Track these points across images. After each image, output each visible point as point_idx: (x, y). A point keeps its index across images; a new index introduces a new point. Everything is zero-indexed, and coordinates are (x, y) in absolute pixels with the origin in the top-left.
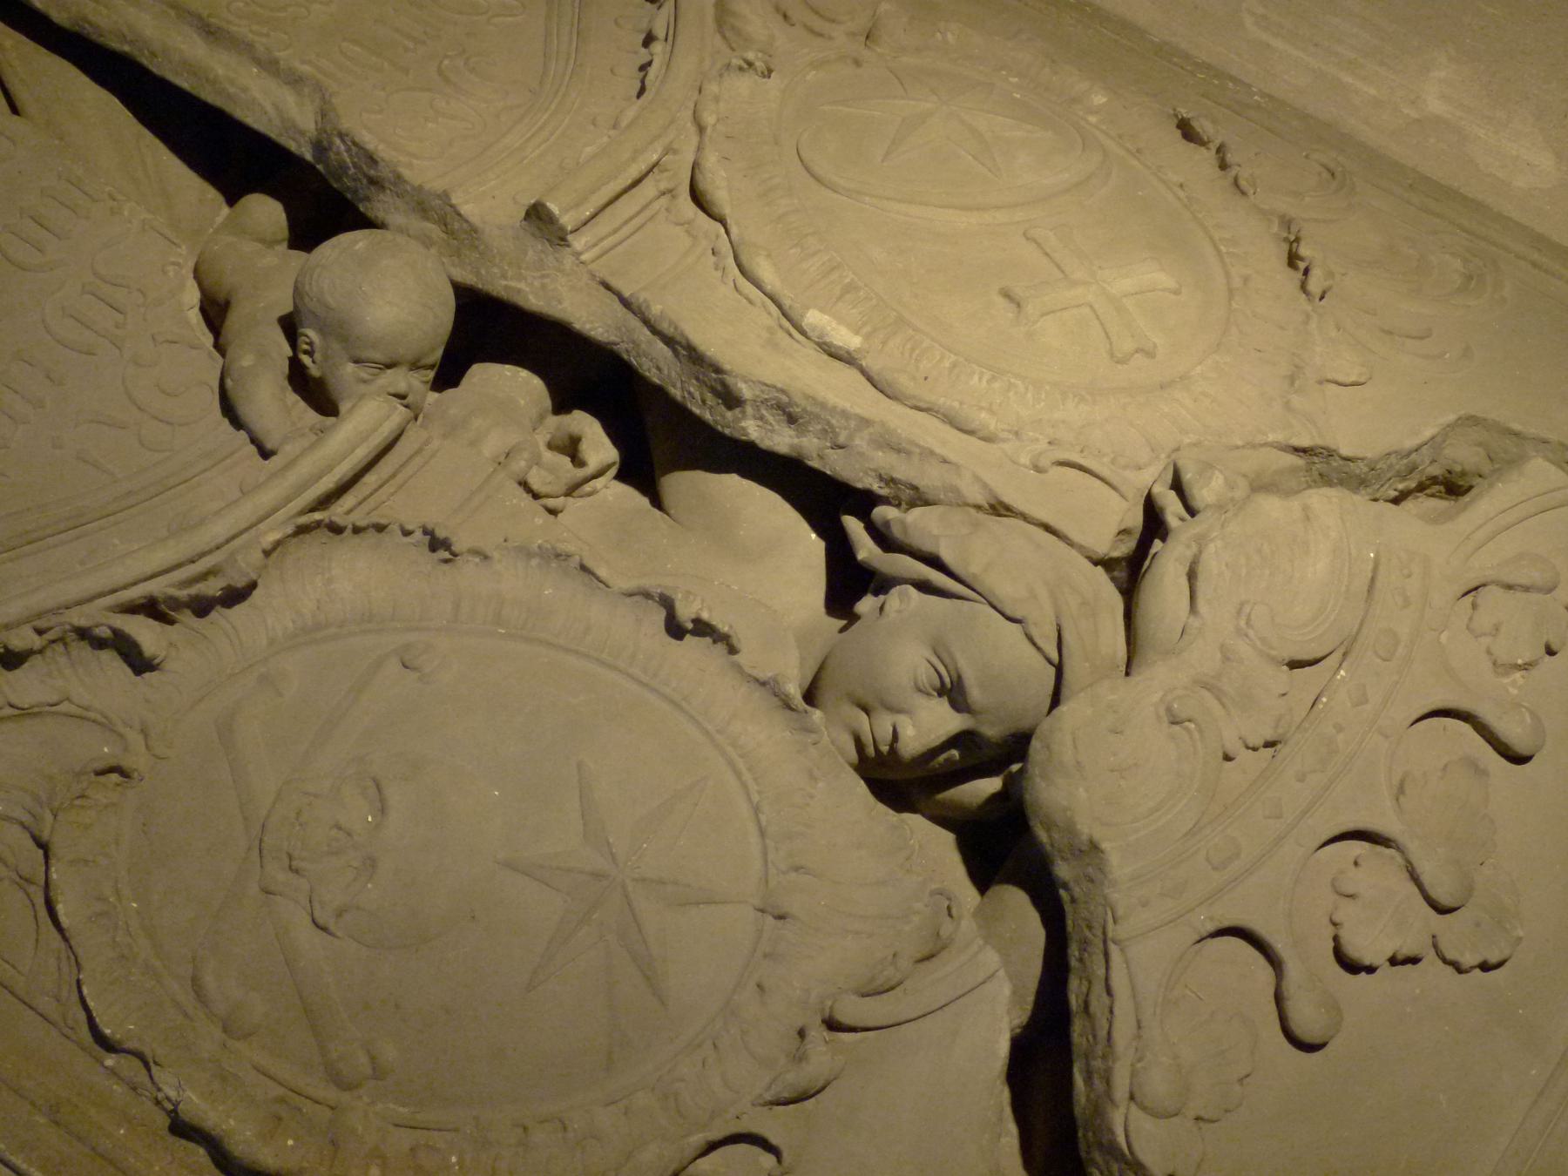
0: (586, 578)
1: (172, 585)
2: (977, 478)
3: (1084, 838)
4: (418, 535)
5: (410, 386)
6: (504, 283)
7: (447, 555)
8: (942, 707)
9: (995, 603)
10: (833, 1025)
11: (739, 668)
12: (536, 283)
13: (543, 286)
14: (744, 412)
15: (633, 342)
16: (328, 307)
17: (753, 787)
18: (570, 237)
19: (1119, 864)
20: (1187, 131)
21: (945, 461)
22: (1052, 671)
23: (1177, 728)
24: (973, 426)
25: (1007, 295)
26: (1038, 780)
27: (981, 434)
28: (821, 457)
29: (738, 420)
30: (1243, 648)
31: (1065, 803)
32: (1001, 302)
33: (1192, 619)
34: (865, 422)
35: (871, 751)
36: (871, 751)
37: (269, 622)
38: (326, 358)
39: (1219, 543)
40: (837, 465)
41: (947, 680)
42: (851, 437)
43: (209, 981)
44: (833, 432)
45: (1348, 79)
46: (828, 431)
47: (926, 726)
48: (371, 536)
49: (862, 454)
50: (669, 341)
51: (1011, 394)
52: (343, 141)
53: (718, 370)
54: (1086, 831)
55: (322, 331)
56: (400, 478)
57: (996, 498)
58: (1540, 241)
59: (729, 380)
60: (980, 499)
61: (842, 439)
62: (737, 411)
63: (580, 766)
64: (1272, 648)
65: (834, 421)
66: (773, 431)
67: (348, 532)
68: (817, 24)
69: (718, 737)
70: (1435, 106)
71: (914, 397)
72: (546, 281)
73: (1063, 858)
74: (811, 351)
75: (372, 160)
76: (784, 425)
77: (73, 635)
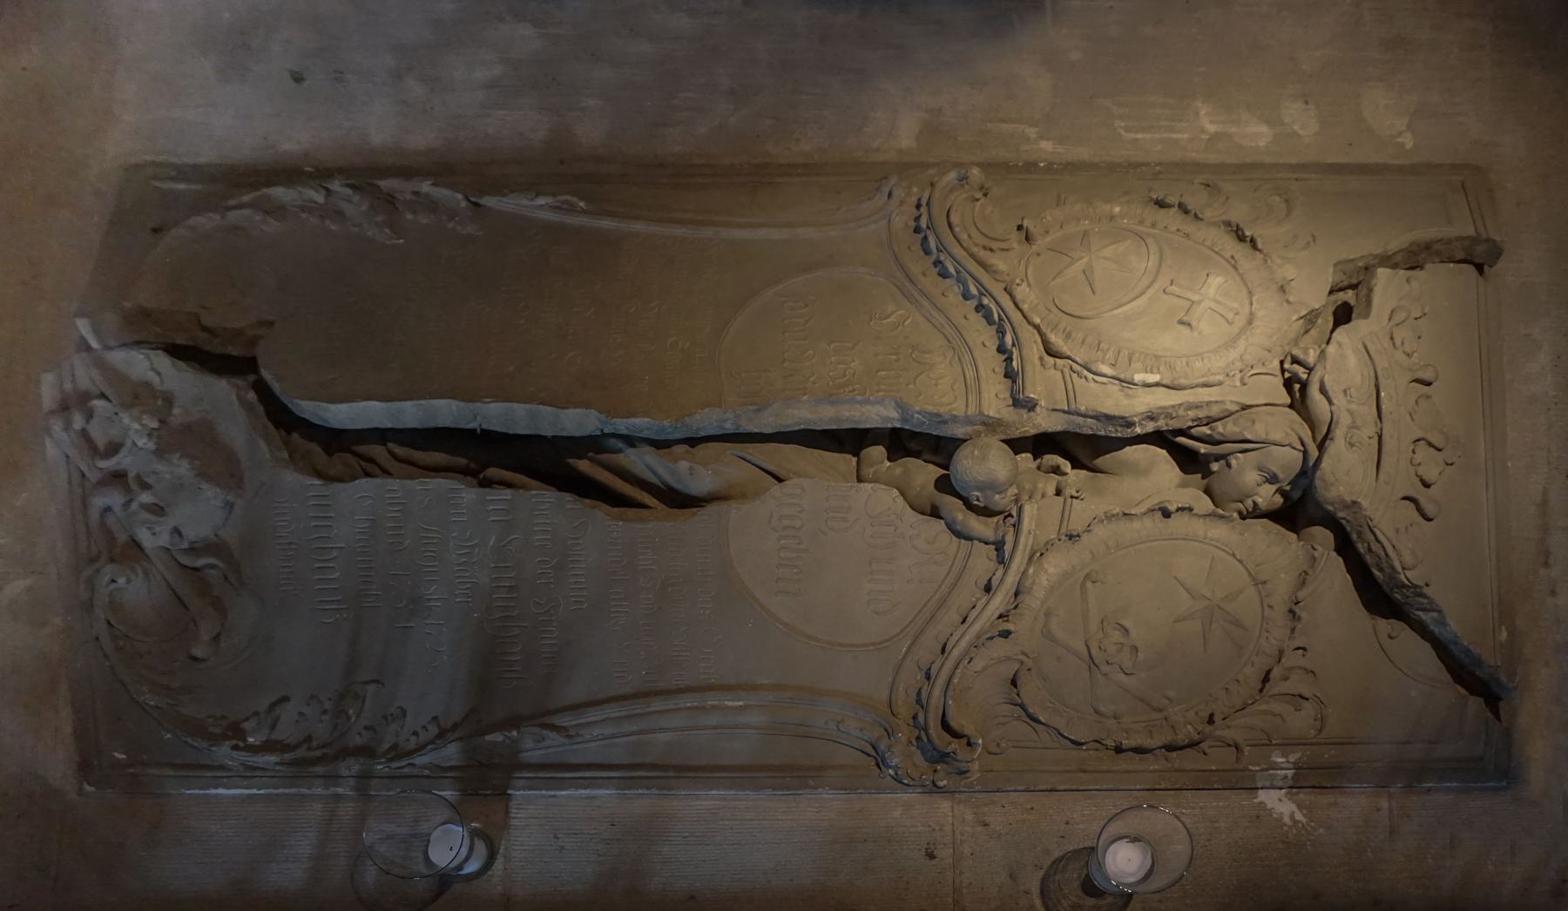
8: (1267, 486)
20: (1161, 204)
25: (1181, 322)
30: (1353, 406)
32: (1181, 327)
43: (1102, 709)
45: (1174, 136)
47: (1267, 496)
58: (1292, 168)
68: (1002, 245)
70: (1212, 128)
74: (1141, 390)
75: (938, 415)
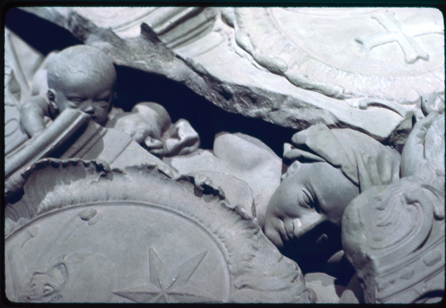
0: (161, 175)
2: (331, 113)
3: (140, 166)
5: (94, 108)
9: (328, 160)
11: (223, 205)
12: (149, 60)
13: (152, 61)
14: (233, 100)
17: (227, 254)
18: (160, 37)
19: (380, 268)
21: (317, 108)
23: (411, 206)
24: (333, 92)
27: (337, 96)
29: (232, 104)
31: (356, 242)
32: (355, 44)
34: (285, 97)
35: (286, 237)
36: (286, 237)
37: (30, 208)
39: (436, 126)
40: (277, 118)
42: (279, 105)
44: (271, 103)
46: (269, 104)
48: (71, 168)
49: (284, 111)
50: (201, 74)
51: (355, 80)
53: (220, 82)
56: (89, 146)
57: (338, 120)
59: (224, 86)
60: (332, 122)
61: (275, 106)
62: (231, 100)
65: (271, 99)
66: (247, 107)
67: (61, 167)
72: (153, 58)
76: (252, 104)
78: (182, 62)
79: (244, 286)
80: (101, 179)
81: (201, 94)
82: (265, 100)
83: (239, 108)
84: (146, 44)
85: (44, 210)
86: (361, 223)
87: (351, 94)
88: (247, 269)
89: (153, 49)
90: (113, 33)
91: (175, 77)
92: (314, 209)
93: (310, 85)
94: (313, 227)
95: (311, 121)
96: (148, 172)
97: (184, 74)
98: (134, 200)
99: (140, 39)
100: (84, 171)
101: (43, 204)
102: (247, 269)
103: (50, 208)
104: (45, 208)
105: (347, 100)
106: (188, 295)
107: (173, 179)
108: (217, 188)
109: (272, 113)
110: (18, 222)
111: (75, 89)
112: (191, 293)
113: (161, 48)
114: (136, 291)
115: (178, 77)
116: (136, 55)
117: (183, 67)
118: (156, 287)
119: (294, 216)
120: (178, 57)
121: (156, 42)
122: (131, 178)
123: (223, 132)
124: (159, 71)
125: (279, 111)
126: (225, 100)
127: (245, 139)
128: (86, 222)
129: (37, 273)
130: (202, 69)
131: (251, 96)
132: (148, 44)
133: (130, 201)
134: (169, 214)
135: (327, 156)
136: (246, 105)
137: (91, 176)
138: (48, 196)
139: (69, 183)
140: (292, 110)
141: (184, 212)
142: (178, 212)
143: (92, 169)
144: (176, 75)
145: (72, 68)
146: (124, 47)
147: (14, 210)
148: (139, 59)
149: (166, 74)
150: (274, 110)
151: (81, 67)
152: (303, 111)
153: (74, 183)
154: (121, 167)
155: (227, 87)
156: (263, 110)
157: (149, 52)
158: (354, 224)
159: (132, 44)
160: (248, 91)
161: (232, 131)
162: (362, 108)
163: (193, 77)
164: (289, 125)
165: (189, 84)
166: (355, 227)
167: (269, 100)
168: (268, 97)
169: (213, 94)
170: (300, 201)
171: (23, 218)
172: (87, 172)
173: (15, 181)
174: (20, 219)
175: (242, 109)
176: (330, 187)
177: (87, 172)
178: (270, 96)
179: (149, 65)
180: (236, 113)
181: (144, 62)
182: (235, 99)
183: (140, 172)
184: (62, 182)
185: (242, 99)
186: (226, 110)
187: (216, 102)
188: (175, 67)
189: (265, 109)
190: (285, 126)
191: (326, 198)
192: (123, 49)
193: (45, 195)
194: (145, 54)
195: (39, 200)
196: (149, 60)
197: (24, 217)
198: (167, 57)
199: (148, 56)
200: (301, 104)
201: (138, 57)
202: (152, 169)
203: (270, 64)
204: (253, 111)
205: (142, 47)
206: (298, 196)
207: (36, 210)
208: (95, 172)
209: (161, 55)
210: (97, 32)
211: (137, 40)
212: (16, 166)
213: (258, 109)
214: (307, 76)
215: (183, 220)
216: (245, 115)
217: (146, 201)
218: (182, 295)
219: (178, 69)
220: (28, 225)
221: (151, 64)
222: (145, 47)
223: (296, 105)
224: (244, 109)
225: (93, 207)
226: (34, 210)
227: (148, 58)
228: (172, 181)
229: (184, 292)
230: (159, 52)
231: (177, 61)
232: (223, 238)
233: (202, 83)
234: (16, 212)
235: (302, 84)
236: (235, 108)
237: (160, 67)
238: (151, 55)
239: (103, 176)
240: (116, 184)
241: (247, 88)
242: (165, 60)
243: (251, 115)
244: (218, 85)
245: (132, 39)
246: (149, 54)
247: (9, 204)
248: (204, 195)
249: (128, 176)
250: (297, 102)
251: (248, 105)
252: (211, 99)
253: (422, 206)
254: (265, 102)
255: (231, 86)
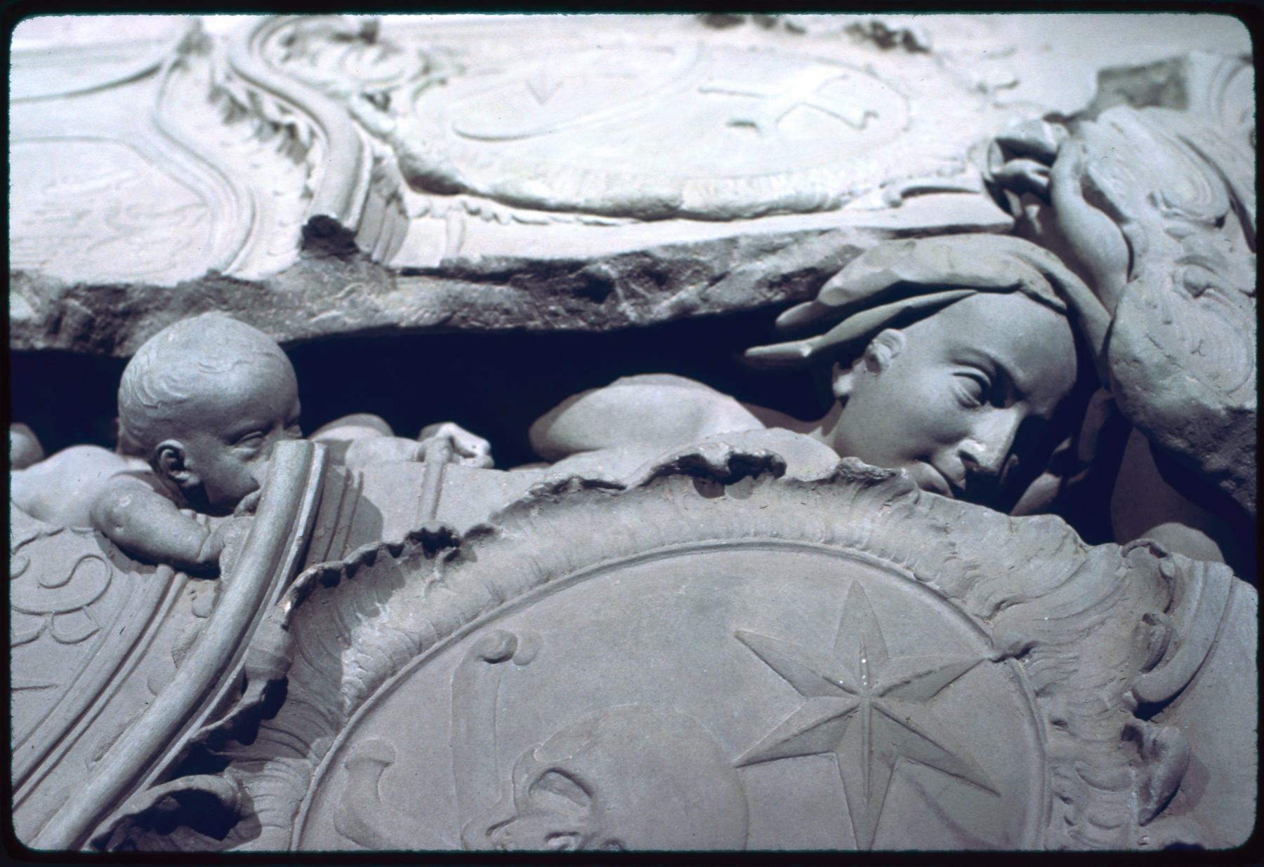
0: (594, 495)
1: (203, 725)
4: (412, 548)
6: (314, 320)
7: (449, 550)
9: (983, 284)
10: (1147, 710)
11: (796, 484)
12: (345, 303)
13: (353, 304)
15: (466, 305)
16: (181, 402)
21: (823, 232)
22: (1062, 321)
23: (1202, 299)
26: (1145, 395)
28: (705, 300)
33: (1126, 228)
37: (321, 708)
38: (199, 458)
41: (986, 378)
52: (76, 297)
54: (1219, 407)
55: (179, 434)
56: (344, 522)
59: (591, 269)
63: (738, 636)
64: (1200, 215)
65: (702, 258)
66: (647, 302)
69: (833, 547)
71: (750, 206)
72: (354, 295)
73: (1209, 451)
77: (137, 830)
78: (425, 278)
79: (998, 607)
80: (449, 569)
81: (509, 326)
82: (688, 268)
83: (629, 310)
84: (326, 269)
85: (361, 698)
86: (1168, 357)
87: (851, 193)
88: (970, 573)
89: (346, 275)
90: (230, 280)
91: (420, 318)
92: (988, 405)
93: (759, 205)
94: (1012, 437)
95: (822, 262)
96: (556, 502)
97: (444, 302)
98: (571, 571)
99: (306, 264)
100: (395, 568)
101: (350, 683)
102: (970, 573)
103: (373, 685)
104: (360, 690)
105: (847, 207)
106: (920, 676)
107: (629, 488)
108: (764, 453)
109: (713, 288)
110: (311, 755)
111: (245, 408)
112: (921, 669)
113: (364, 266)
114: (795, 730)
115: (427, 315)
116: (309, 304)
117: (431, 289)
118: (835, 699)
119: (952, 438)
120: (410, 272)
121: (350, 254)
122: (517, 535)
123: (574, 397)
124: (378, 321)
125: (729, 277)
126: (594, 306)
127: (645, 383)
128: (511, 663)
129: (494, 827)
130: (504, 264)
131: (653, 272)
132: (331, 267)
133: (562, 578)
134: (687, 559)
135: (979, 278)
136: (643, 297)
137: (414, 573)
138: (345, 661)
139: (376, 613)
140: (759, 263)
141: (716, 537)
142: (703, 543)
143: (414, 556)
144: (421, 312)
145: (214, 364)
146: (267, 298)
147: (281, 731)
148: (321, 311)
149: (395, 320)
150: (715, 280)
151: (235, 355)
152: (790, 253)
153: (387, 606)
154: (483, 519)
155: (599, 269)
156: (688, 294)
157: (340, 285)
158: (1157, 365)
159: (287, 284)
160: (647, 260)
161: (604, 379)
162: (895, 205)
163: (475, 295)
164: (763, 299)
165: (464, 319)
166: (1164, 372)
167: (697, 262)
168: (695, 257)
169: (552, 308)
170: (964, 399)
171: (319, 740)
172: (403, 570)
173: (277, 648)
174: (313, 746)
175: (635, 310)
176: (1021, 334)
177: (403, 570)
178: (698, 254)
179: (351, 316)
180: (625, 324)
181: (334, 313)
182: (620, 291)
183: (534, 513)
184: (360, 615)
185: (633, 286)
186: (597, 328)
187: (565, 320)
188: (410, 299)
189: (691, 288)
190: (756, 303)
191: (1023, 362)
192: (270, 304)
193: (338, 661)
194: (330, 294)
195: (335, 679)
196: (345, 303)
197: (319, 736)
198: (381, 282)
199: (341, 294)
200: (777, 241)
201: (315, 308)
202: (566, 489)
203: (640, 201)
204: (663, 306)
205: (318, 279)
206: (952, 391)
207: (341, 705)
208: (422, 559)
209: (368, 282)
210: (168, 299)
211: (295, 270)
212: (244, 619)
213: (674, 294)
214: (736, 193)
215: (732, 553)
216: (646, 323)
217: (604, 558)
218: (908, 682)
219: (422, 299)
220: (342, 749)
221: (354, 311)
222: (326, 278)
223: (769, 248)
224: (639, 308)
225: (500, 625)
226: (334, 709)
227: (341, 299)
228: (630, 492)
229: (907, 675)
230: (362, 276)
231: (407, 284)
232: (857, 542)
233: (509, 297)
234: (290, 734)
235: (741, 209)
236: (622, 314)
237: (376, 311)
238: (347, 289)
239: (449, 559)
240: (489, 561)
241: (644, 254)
242: (379, 293)
243: (659, 317)
244: (572, 276)
245: (282, 272)
246: (341, 289)
247: (263, 722)
248: (727, 488)
249: (505, 532)
250: (766, 242)
251: (649, 296)
252: (547, 323)
253: (1221, 291)
254: (689, 272)
255: (607, 263)
